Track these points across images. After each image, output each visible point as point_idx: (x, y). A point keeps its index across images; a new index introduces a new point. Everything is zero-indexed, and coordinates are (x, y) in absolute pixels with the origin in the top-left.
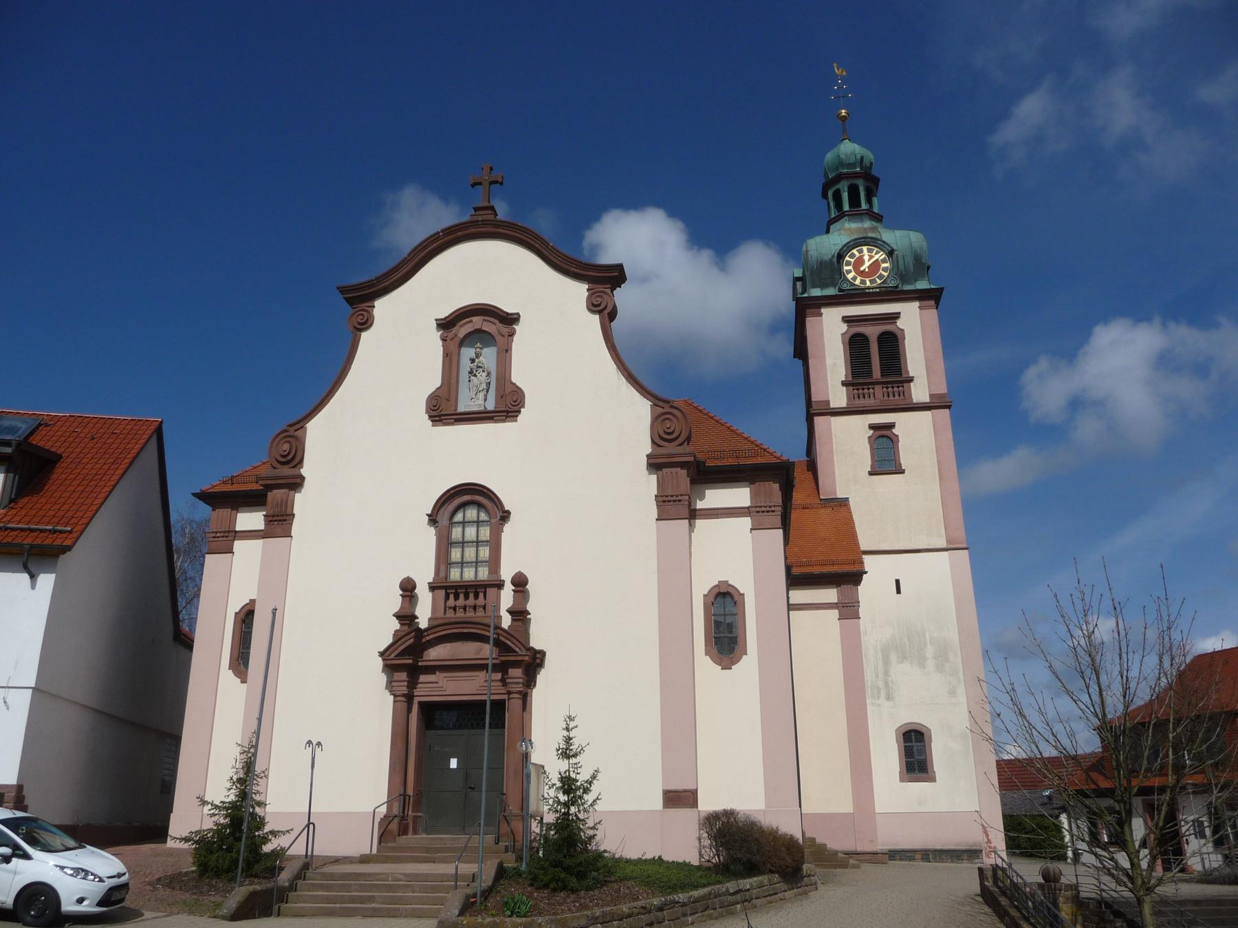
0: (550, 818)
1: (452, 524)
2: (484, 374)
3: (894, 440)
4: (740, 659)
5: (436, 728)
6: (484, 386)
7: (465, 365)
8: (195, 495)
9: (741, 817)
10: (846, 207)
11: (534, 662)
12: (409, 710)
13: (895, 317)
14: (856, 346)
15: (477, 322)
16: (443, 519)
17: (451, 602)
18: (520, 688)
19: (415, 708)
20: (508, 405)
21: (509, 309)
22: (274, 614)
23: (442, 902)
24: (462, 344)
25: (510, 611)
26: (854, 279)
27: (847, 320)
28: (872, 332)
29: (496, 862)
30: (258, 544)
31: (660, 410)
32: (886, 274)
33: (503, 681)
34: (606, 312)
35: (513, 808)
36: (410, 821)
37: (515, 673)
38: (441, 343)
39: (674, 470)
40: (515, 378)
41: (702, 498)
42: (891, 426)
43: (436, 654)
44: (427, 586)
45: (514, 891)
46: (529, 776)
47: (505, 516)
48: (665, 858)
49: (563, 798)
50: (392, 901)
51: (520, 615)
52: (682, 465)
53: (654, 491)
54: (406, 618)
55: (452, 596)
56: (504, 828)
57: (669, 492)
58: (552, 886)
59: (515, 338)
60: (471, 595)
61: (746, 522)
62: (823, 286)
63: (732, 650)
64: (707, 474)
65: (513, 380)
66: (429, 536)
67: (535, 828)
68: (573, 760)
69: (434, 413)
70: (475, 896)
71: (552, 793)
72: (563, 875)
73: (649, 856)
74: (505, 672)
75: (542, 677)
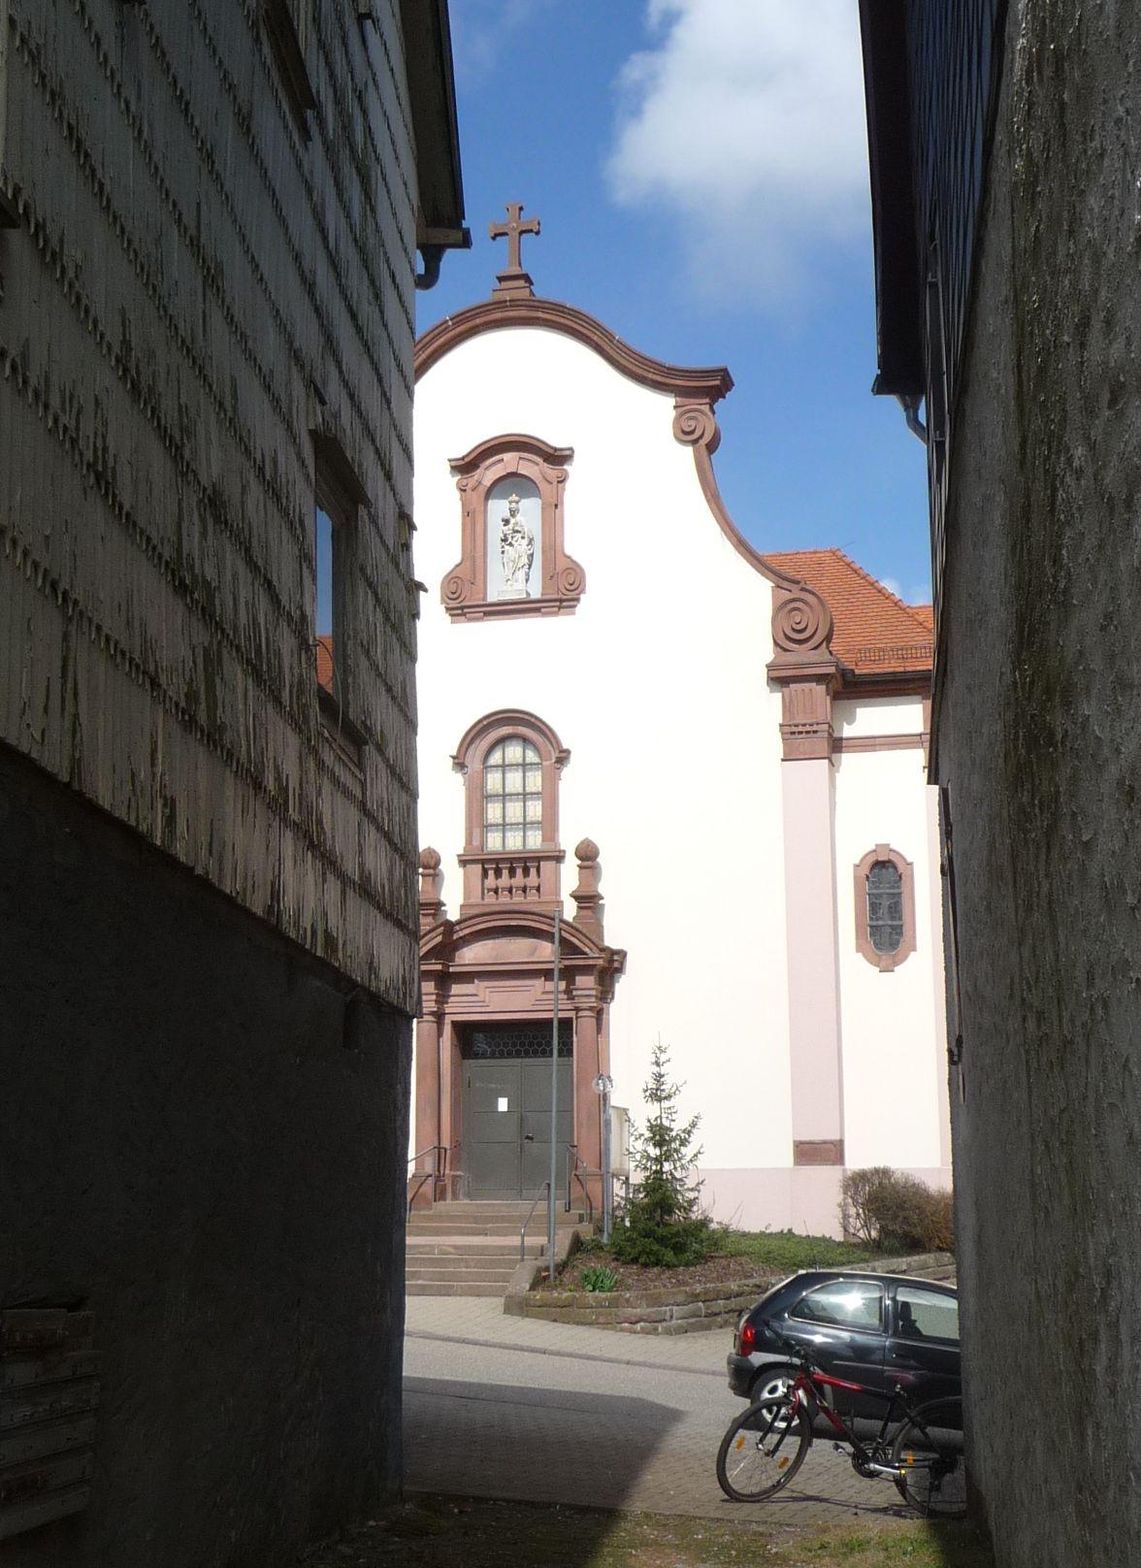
0: (637, 1178)
1: (486, 768)
4: (906, 957)
5: (476, 1056)
6: (525, 560)
7: (495, 530)
9: (898, 1175)
11: (610, 967)
12: (440, 1034)
15: (510, 461)
16: (474, 762)
17: (491, 881)
18: (593, 1003)
19: (448, 1029)
20: (562, 590)
21: (556, 440)
23: (505, 1278)
24: (489, 493)
25: (576, 897)
29: (571, 1230)
31: (788, 596)
33: (568, 992)
34: (703, 442)
35: (588, 1164)
36: (448, 1182)
38: (457, 494)
39: (806, 686)
40: (570, 549)
41: (851, 720)
43: (471, 955)
44: (456, 860)
45: (593, 1265)
46: (608, 1123)
47: (563, 757)
48: (796, 1232)
49: (654, 1152)
50: (442, 1277)
51: (589, 901)
52: (819, 679)
55: (491, 873)
56: (577, 1191)
58: (642, 1260)
59: (568, 484)
60: (519, 871)
63: (894, 945)
64: (854, 687)
65: (567, 551)
67: (619, 1190)
68: (666, 1104)
69: (453, 604)
70: (547, 1269)
71: (639, 1145)
72: (656, 1247)
73: (775, 1229)
74: (571, 981)
75: (622, 986)
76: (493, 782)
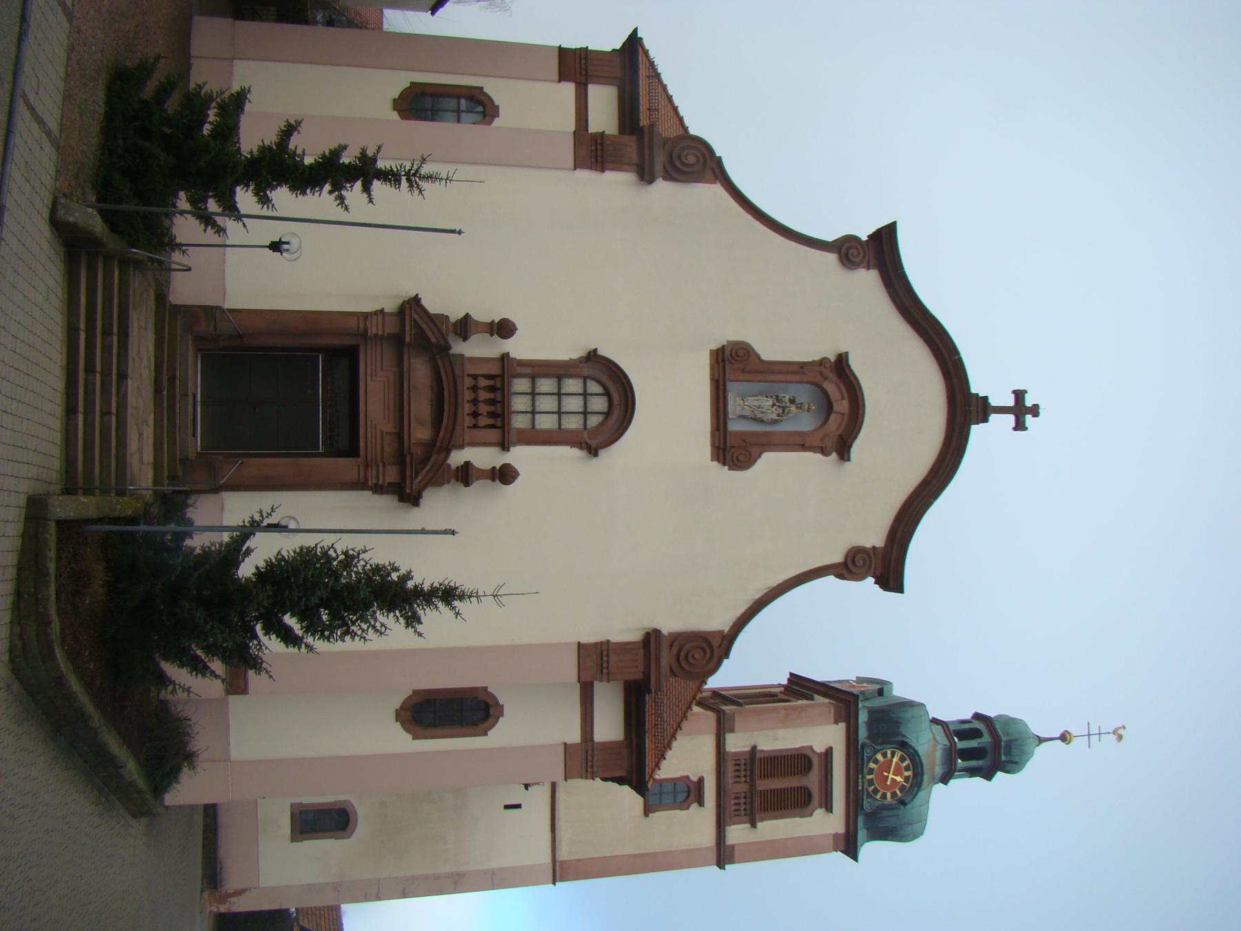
2: (774, 417)
3: (684, 805)
8: (635, 31)
10: (961, 745)
13: (829, 808)
14: (799, 761)
15: (842, 406)
17: (483, 383)
21: (857, 448)
22: (446, 532)
26: (876, 761)
27: (829, 753)
28: (813, 781)
30: (569, 124)
32: (878, 797)
37: (392, 475)
38: (817, 358)
42: (701, 803)
47: (593, 451)
51: (466, 475)
52: (647, 675)
53: (616, 637)
54: (465, 327)
55: (490, 383)
57: (613, 658)
61: (575, 736)
62: (869, 724)
66: (566, 350)
69: (727, 352)
76: (573, 385)
